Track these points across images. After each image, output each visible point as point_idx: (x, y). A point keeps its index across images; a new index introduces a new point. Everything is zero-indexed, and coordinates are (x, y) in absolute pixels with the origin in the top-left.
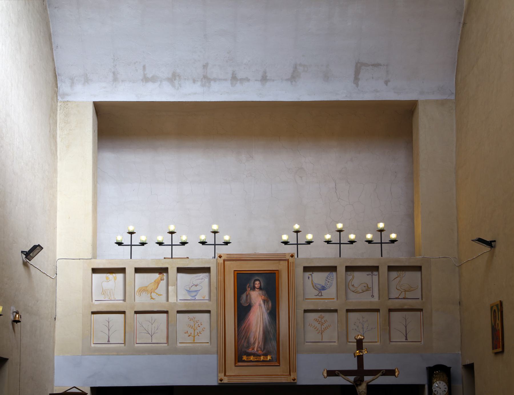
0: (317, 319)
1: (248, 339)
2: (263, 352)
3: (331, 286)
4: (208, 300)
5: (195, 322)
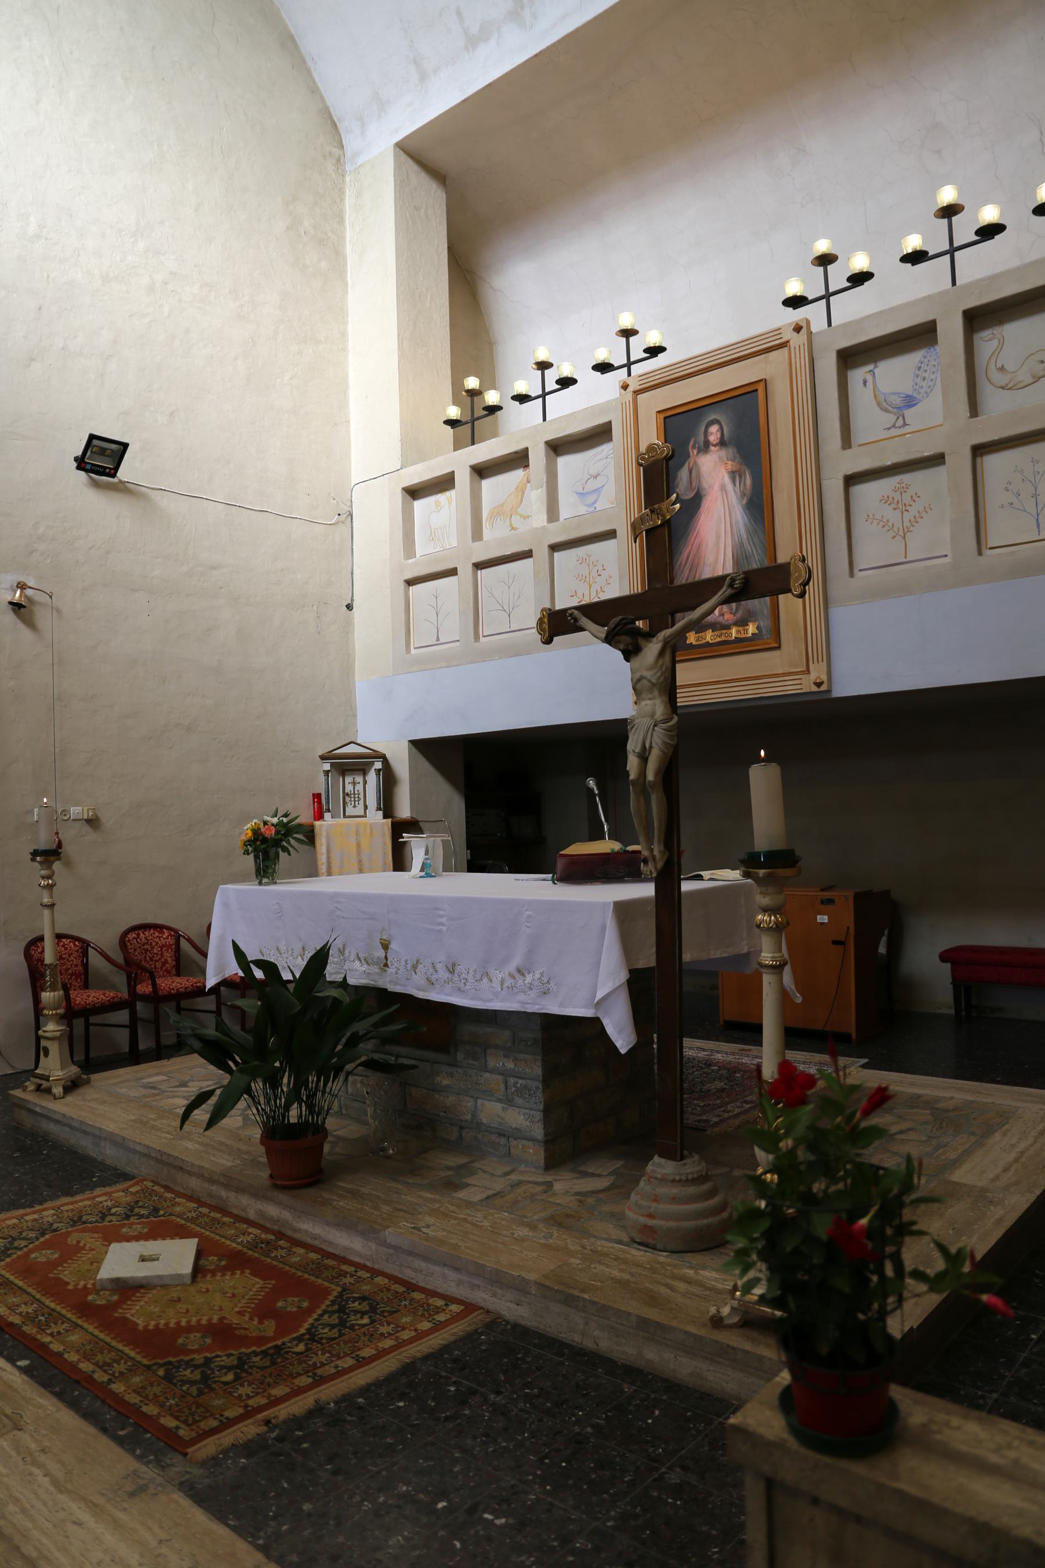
0: (888, 497)
2: (734, 615)
3: (932, 390)
5: (591, 566)
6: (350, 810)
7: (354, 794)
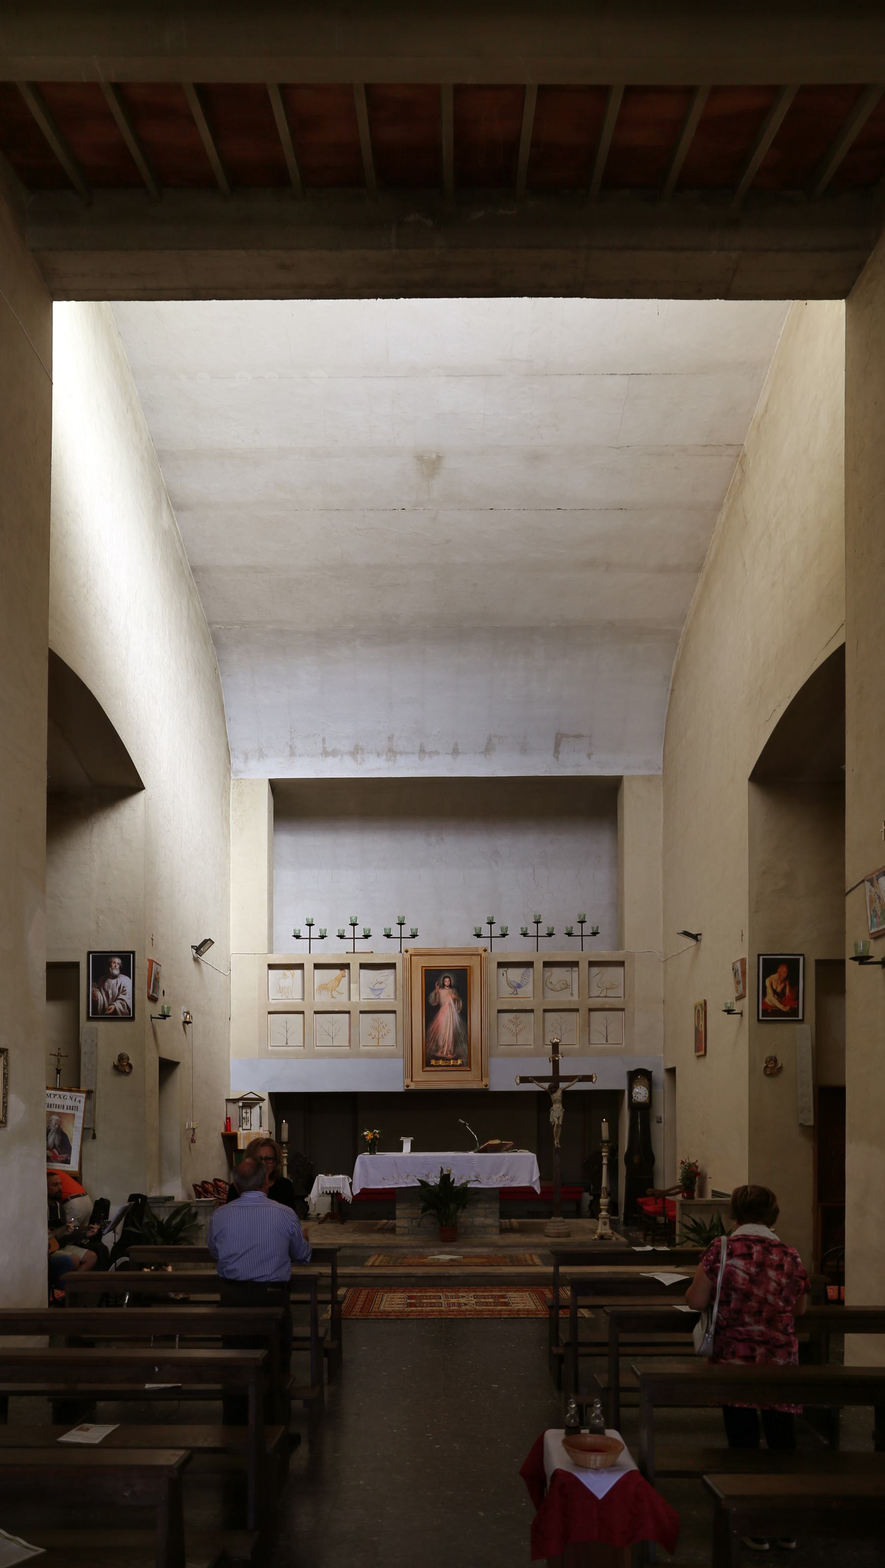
2: (452, 1055)
5: (379, 1023)
6: (245, 1127)
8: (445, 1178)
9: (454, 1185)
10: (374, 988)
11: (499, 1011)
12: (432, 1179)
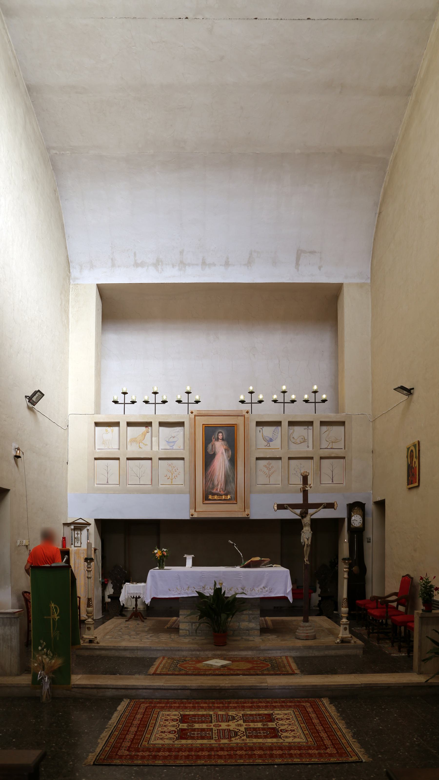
1: (212, 481)
2: (224, 492)
4: (183, 449)
5: (173, 468)
6: (76, 544)
7: (78, 538)
8: (218, 591)
9: (225, 596)
10: (169, 441)
11: (257, 459)
12: (207, 591)
